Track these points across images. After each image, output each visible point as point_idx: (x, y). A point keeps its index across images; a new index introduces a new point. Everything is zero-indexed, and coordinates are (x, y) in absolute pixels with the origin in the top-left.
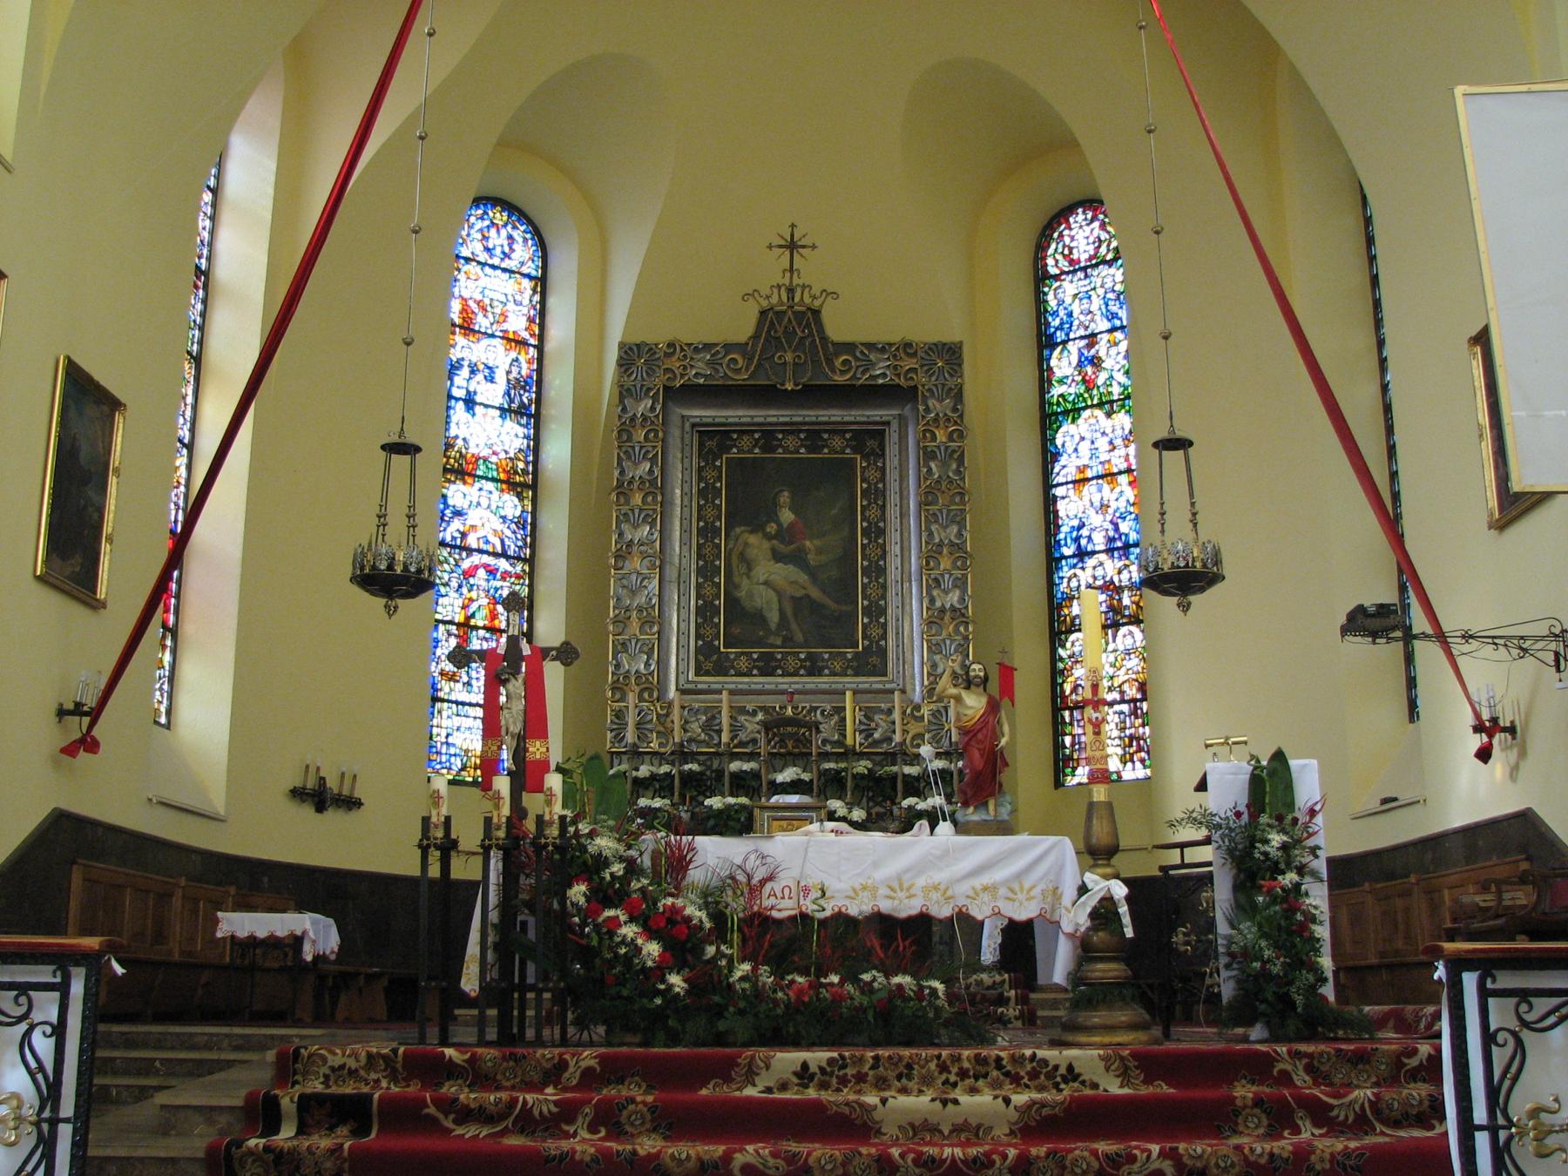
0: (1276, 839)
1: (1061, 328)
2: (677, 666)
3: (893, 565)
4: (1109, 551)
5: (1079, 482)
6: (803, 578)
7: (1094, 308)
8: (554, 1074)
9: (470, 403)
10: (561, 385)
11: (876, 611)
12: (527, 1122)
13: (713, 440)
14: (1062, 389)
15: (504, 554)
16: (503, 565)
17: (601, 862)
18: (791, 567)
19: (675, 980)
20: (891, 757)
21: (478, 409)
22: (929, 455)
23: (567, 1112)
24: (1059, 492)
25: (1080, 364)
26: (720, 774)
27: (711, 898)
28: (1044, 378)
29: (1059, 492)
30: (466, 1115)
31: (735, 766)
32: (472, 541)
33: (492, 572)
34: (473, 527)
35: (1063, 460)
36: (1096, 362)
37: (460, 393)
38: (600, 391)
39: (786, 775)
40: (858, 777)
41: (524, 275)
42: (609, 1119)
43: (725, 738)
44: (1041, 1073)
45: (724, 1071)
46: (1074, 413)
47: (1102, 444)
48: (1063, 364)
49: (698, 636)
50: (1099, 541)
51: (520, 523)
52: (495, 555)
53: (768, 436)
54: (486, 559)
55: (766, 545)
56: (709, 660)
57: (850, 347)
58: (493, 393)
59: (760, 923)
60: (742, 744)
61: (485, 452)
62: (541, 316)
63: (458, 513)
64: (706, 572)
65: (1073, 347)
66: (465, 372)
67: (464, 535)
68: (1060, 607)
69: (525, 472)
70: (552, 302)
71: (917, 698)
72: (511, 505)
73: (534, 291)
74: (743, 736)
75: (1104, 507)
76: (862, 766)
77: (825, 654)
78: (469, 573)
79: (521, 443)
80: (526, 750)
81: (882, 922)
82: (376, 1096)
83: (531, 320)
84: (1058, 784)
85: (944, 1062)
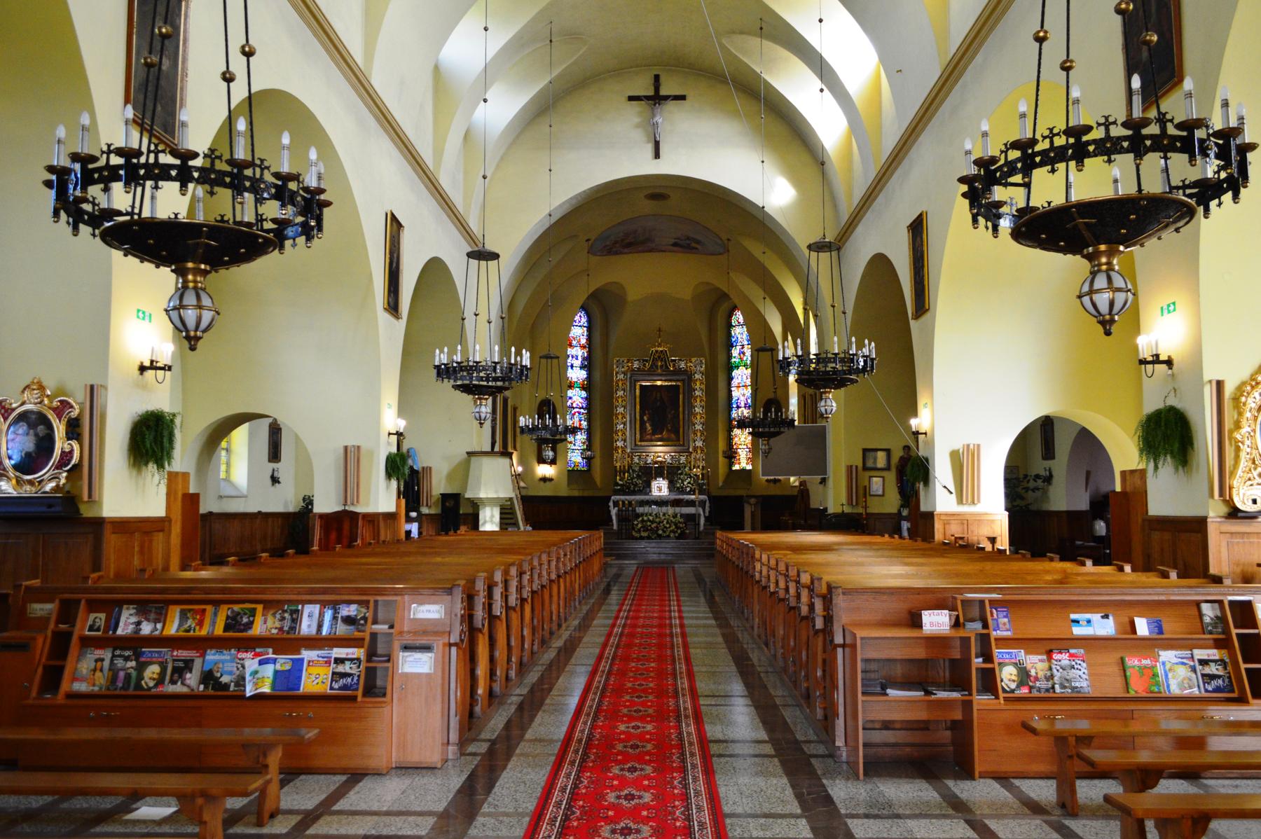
4: (745, 407)
9: (572, 366)
15: (582, 408)
16: (582, 411)
24: (733, 389)
25: (740, 354)
28: (730, 356)
32: (574, 405)
33: (579, 413)
35: (734, 380)
36: (744, 353)
37: (569, 364)
46: (737, 367)
47: (744, 377)
50: (743, 405)
51: (586, 398)
52: (580, 408)
54: (578, 410)
58: (577, 363)
61: (576, 380)
62: (589, 338)
63: (570, 398)
65: (738, 348)
66: (570, 358)
72: (584, 394)
75: (744, 395)
78: (574, 414)
79: (585, 376)
80: (548, 444)
85: (664, 467)
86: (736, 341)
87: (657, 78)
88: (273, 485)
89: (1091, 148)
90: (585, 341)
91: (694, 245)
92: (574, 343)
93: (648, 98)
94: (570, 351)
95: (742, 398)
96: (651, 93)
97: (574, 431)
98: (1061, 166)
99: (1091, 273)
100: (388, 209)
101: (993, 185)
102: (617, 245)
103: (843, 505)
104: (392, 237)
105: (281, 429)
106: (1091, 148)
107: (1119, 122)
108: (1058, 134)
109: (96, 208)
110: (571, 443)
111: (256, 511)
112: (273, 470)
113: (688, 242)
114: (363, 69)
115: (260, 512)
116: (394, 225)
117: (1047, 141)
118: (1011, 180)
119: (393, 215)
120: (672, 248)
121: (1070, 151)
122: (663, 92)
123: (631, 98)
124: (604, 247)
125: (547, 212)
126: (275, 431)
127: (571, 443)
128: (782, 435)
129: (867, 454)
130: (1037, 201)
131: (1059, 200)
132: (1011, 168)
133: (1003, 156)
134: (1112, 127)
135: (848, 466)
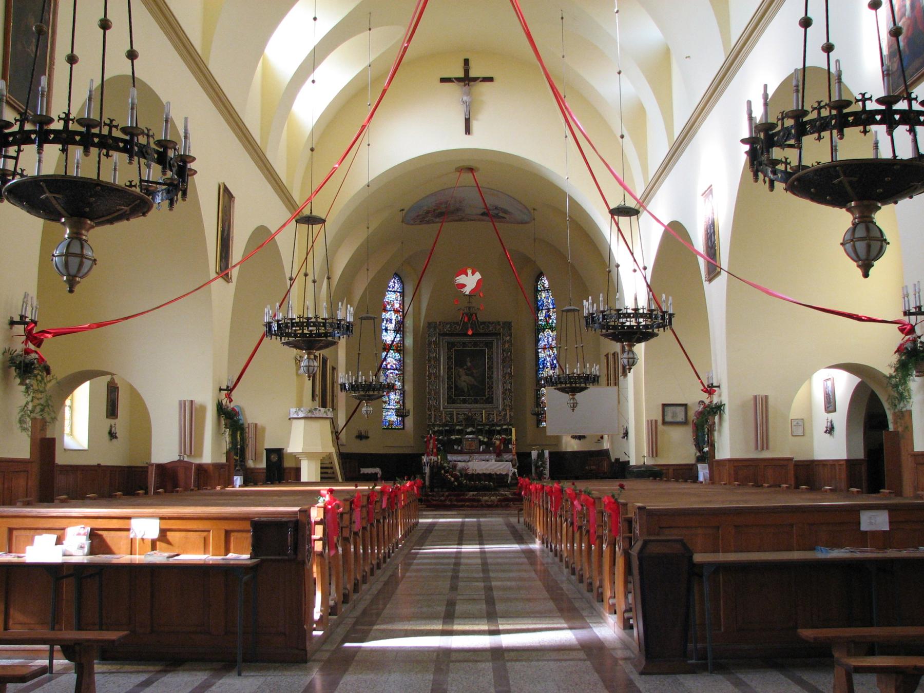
0: (540, 463)
1: (541, 305)
2: (443, 403)
3: (495, 376)
5: (544, 349)
6: (473, 380)
7: (549, 301)
8: (443, 496)
9: (386, 330)
10: (409, 323)
11: (491, 388)
12: (441, 501)
13: (451, 345)
14: (541, 323)
15: (396, 369)
16: (396, 372)
17: (445, 467)
18: (470, 377)
19: (456, 483)
20: (493, 425)
21: (389, 332)
22: (504, 351)
23: (445, 500)
25: (545, 316)
26: (454, 430)
27: (460, 471)
28: (537, 319)
29: (539, 350)
30: (434, 500)
31: (457, 427)
34: (389, 363)
36: (550, 317)
37: (384, 328)
38: (420, 326)
39: (469, 430)
40: (486, 430)
41: (398, 292)
42: (450, 500)
43: (455, 420)
44: (502, 495)
45: (463, 495)
46: (543, 330)
48: (542, 316)
49: (448, 394)
51: (400, 360)
52: (394, 370)
53: (464, 344)
54: (392, 371)
55: (464, 371)
56: (451, 400)
57: (484, 323)
58: (391, 326)
59: (467, 475)
60: (459, 422)
62: (402, 303)
64: (449, 378)
66: (385, 322)
67: (386, 365)
68: (539, 381)
69: (401, 346)
70: (405, 299)
71: (500, 409)
73: (401, 296)
74: (459, 420)
75: (550, 356)
76: (487, 428)
77: (478, 398)
81: (484, 475)
82: (316, 514)
83: (400, 304)
84: (538, 426)
86: (542, 305)
87: (466, 62)
88: (111, 440)
89: (851, 119)
90: (398, 305)
91: (501, 214)
92: (388, 307)
93: (459, 80)
94: (387, 315)
95: (548, 359)
96: (461, 74)
97: (391, 388)
98: (826, 134)
99: (853, 224)
100: (221, 181)
101: (772, 147)
102: (430, 215)
103: (644, 457)
104: (224, 207)
105: (118, 388)
106: (851, 119)
107: (874, 99)
108: (824, 107)
109: (151, 140)
110: (385, 402)
111: (95, 463)
112: (111, 426)
113: (496, 212)
114: (201, 55)
115: (99, 465)
116: (226, 196)
117: (816, 112)
118: (788, 142)
119: (225, 187)
120: (481, 217)
121: (833, 122)
122: (473, 74)
123: (443, 80)
124: (418, 216)
125: (366, 182)
126: (113, 390)
127: (385, 402)
128: (589, 389)
129: (666, 408)
130: (809, 161)
131: (826, 159)
132: (786, 132)
133: (780, 123)
134: (868, 103)
135: (648, 421)
